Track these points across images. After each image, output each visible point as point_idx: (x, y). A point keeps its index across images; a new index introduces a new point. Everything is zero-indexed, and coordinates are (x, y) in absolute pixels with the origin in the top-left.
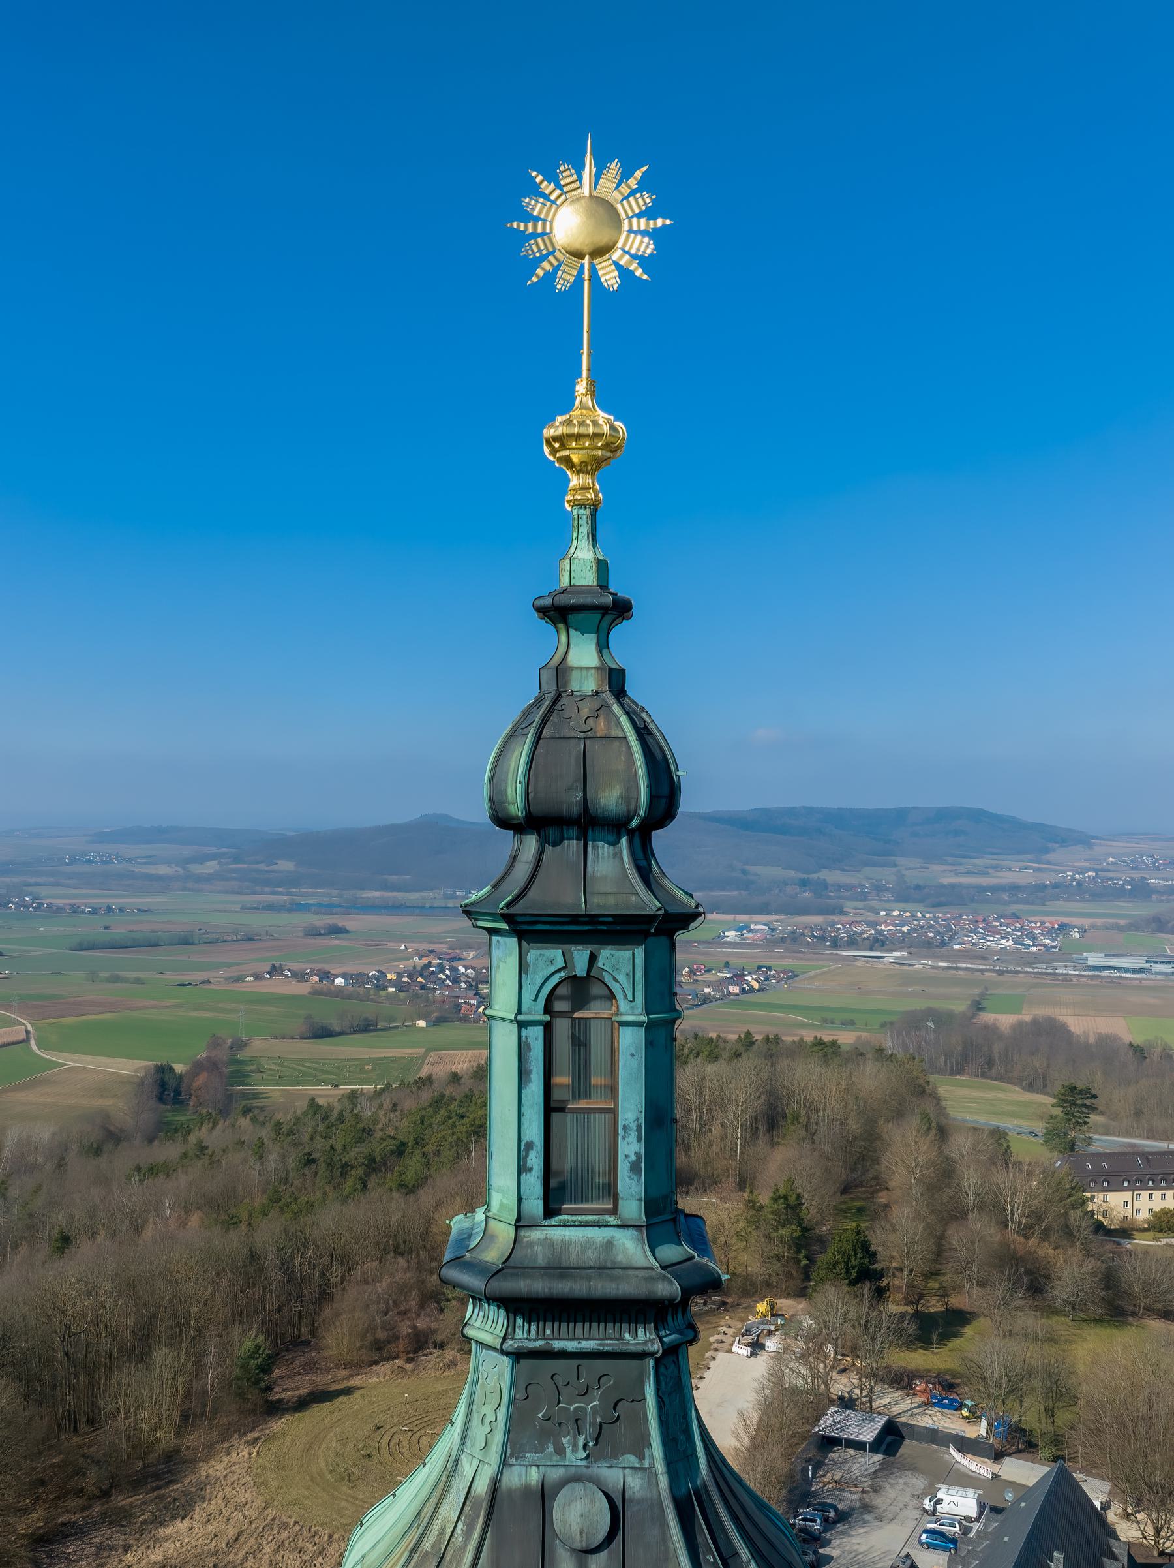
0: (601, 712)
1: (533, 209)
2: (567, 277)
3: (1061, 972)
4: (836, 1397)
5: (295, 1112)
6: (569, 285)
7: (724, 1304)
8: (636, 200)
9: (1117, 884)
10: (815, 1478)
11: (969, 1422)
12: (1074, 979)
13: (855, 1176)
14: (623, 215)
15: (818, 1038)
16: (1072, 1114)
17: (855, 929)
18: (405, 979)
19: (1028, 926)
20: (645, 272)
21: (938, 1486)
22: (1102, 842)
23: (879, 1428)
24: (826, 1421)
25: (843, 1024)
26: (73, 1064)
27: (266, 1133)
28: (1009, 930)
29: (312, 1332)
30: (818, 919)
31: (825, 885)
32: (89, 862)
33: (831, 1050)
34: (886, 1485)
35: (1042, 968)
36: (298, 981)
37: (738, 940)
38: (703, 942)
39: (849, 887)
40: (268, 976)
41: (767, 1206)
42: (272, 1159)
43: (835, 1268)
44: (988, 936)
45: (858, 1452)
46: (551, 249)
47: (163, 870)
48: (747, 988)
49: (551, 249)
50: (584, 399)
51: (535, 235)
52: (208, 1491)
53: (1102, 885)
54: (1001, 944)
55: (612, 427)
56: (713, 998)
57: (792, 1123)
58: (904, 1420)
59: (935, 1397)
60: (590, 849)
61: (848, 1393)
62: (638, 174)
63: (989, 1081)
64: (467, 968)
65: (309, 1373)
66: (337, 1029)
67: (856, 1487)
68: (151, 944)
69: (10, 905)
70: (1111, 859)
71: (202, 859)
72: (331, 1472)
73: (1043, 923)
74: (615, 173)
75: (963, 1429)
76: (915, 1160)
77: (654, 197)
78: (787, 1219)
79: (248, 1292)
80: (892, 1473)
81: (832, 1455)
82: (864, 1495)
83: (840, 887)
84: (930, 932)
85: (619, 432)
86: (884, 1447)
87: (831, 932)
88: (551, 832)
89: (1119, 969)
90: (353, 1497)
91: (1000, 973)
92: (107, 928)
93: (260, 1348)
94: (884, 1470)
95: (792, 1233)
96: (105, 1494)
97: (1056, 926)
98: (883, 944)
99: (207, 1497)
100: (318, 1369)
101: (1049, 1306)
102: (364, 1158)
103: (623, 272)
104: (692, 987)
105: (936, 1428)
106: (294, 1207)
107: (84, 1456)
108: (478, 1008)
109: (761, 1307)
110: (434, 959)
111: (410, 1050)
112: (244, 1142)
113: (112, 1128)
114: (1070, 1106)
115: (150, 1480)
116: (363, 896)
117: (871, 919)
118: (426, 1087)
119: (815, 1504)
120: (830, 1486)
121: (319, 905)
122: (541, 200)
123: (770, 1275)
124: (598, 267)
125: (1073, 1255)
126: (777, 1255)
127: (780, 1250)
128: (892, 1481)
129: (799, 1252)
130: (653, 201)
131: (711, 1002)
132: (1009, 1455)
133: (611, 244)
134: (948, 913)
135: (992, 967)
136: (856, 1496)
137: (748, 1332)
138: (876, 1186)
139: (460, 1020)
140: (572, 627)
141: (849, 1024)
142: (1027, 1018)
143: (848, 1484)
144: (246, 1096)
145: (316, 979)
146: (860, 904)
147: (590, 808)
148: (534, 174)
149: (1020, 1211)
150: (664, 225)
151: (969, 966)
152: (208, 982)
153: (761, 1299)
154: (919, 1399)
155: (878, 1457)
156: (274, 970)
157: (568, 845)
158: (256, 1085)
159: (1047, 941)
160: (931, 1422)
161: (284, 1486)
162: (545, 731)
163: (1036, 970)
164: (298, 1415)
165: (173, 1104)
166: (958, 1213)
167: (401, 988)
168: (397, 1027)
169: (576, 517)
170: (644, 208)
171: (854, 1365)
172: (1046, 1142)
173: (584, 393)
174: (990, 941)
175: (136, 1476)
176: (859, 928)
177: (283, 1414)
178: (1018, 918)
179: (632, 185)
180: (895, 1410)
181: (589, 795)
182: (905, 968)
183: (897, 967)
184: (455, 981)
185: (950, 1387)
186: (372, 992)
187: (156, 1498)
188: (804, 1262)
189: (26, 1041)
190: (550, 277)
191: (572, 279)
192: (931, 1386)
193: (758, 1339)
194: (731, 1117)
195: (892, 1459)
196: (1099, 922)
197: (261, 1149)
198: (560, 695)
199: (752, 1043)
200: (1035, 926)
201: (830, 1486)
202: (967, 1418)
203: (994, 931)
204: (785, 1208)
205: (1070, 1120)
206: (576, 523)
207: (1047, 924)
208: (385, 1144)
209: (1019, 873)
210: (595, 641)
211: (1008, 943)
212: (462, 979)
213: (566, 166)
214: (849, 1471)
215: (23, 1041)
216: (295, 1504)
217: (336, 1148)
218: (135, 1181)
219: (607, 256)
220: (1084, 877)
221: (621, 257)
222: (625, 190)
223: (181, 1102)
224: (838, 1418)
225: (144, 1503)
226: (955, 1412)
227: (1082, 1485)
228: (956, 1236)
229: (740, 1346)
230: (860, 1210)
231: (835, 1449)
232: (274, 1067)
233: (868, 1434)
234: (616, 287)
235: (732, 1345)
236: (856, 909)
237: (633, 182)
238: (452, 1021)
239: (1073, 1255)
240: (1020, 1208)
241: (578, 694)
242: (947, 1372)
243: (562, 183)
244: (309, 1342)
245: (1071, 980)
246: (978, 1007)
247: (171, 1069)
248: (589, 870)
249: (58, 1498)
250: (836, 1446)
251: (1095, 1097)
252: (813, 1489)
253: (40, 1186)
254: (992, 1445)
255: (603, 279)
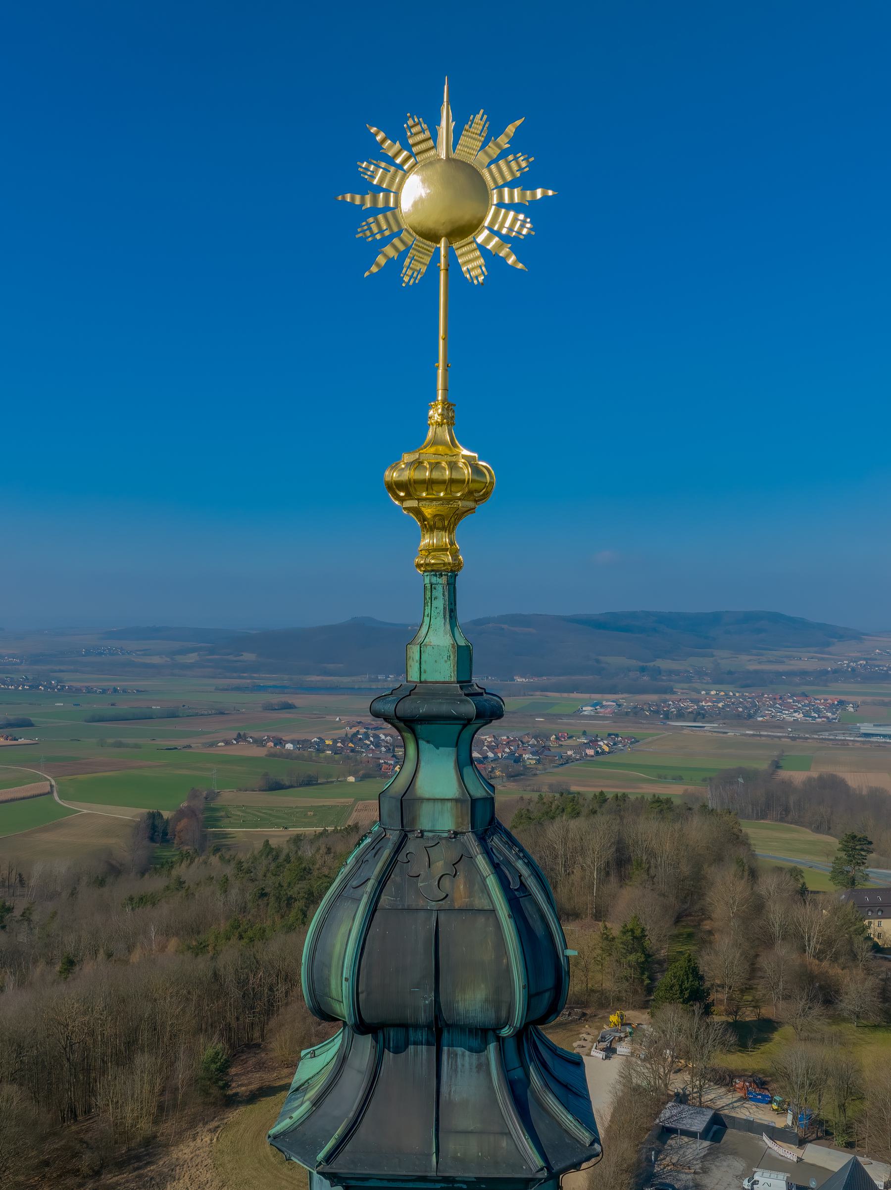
0: (460, 866)
1: (373, 177)
2: (418, 266)
3: (840, 738)
4: (672, 1093)
5: (253, 853)
6: (419, 277)
7: (584, 1014)
8: (508, 164)
9: (882, 670)
10: (658, 1161)
11: (778, 1114)
12: (850, 744)
13: (685, 906)
14: (491, 184)
15: (657, 797)
16: (853, 856)
17: (682, 705)
18: (339, 745)
19: (814, 702)
20: (519, 259)
21: (755, 1169)
22: (870, 637)
23: (708, 1120)
24: (666, 1114)
25: (674, 779)
26: (85, 811)
27: (229, 870)
28: (800, 705)
29: (262, 1036)
30: (653, 698)
31: (659, 671)
32: (100, 654)
33: (666, 806)
34: (713, 1167)
35: (825, 735)
36: (258, 746)
37: (593, 713)
38: (566, 715)
39: (677, 673)
40: (235, 742)
41: (618, 938)
42: (234, 893)
43: (672, 990)
44: (784, 710)
45: (691, 1139)
46: (395, 229)
47: (156, 660)
48: (600, 751)
49: (395, 229)
50: (439, 430)
51: (374, 211)
52: (178, 1171)
53: (871, 671)
54: (794, 717)
55: (476, 470)
56: (574, 758)
57: (637, 869)
58: (726, 1112)
59: (751, 1093)
60: (445, 1057)
61: (682, 1089)
62: (511, 129)
63: (786, 824)
64: (386, 735)
65: (259, 1071)
66: (287, 783)
67: (689, 1169)
68: (147, 717)
69: (40, 687)
70: (877, 651)
71: (184, 652)
72: (274, 1156)
73: (826, 700)
74: (481, 128)
75: (773, 1120)
76: (732, 898)
77: (532, 159)
78: (633, 947)
79: (212, 1007)
80: (718, 1157)
81: (670, 1142)
82: (696, 1176)
83: (670, 672)
84: (740, 707)
85: (485, 476)
86: (711, 1134)
87: (664, 707)
88: (392, 1034)
89: (884, 736)
90: (291, 1177)
91: (793, 739)
92: (113, 705)
93: (219, 1055)
94: (711, 1154)
95: (638, 959)
96: (97, 1174)
97: (836, 703)
98: (704, 716)
99: (177, 1178)
100: (266, 1068)
101: (839, 1015)
102: (305, 893)
103: (491, 258)
104: (558, 750)
105: (752, 1119)
106: (250, 933)
107: (82, 1141)
108: (395, 767)
109: (614, 1018)
110: (361, 729)
111: (342, 800)
112: (213, 878)
113: (114, 862)
114: (852, 850)
115: (133, 1161)
116: (307, 680)
117: (695, 697)
118: (353, 833)
119: (657, 1185)
120: (669, 1168)
121: (275, 687)
122: (383, 165)
123: (620, 992)
124: (458, 252)
125: (857, 974)
126: (626, 976)
127: (629, 972)
128: (718, 1164)
129: (642, 973)
130: (530, 165)
131: (573, 762)
132: (810, 1142)
133: (475, 222)
134: (753, 692)
135: (787, 735)
136: (689, 1176)
137: (603, 1039)
138: (702, 915)
139: (381, 776)
140: (423, 739)
141: (679, 779)
142: (815, 775)
143: (683, 1166)
144: (217, 836)
145: (271, 744)
146: (686, 686)
147: (445, 1015)
148: (373, 130)
149: (815, 939)
150: (545, 197)
151: (770, 733)
152: (189, 747)
153: (613, 1011)
154: (739, 1095)
155: (707, 1143)
156: (240, 738)
157: (416, 1052)
158: (225, 827)
159: (829, 714)
160: (748, 1113)
161: (237, 1168)
162: (383, 897)
163: (821, 737)
164: (250, 1107)
165: (162, 842)
166: (766, 941)
167: (336, 752)
168: (332, 782)
169: (428, 586)
170: (518, 174)
171: (687, 1066)
172: (833, 878)
173: (439, 420)
174: (786, 714)
175: (122, 1157)
176: (685, 704)
177: (238, 1106)
178: (806, 696)
179: (502, 144)
180: (720, 1103)
181: (442, 999)
182: (721, 735)
183: (715, 734)
184: (378, 745)
185: (762, 1084)
186: (314, 754)
187: (136, 1177)
188: (647, 981)
189: (50, 793)
190: (395, 266)
191: (424, 269)
192: (748, 1084)
193: (611, 1045)
194: (589, 863)
195: (717, 1145)
196: (869, 699)
197: (226, 884)
198: (406, 836)
199: (605, 800)
200: (820, 704)
201: (669, 1168)
202: (776, 1110)
203: (789, 707)
204: (633, 940)
205: (852, 861)
206: (428, 594)
207: (829, 701)
208: (321, 882)
209: (807, 661)
210: (453, 758)
211: (799, 716)
212: (383, 744)
213: (416, 120)
214: (684, 1155)
215: (48, 793)
216: (246, 1183)
217: (283, 884)
218: (128, 909)
219: (470, 239)
220: (857, 665)
221: (488, 240)
222: (494, 151)
223: (168, 841)
224: (675, 1112)
225: (127, 1181)
226: (767, 1105)
227: (866, 1168)
228: (766, 962)
229: (597, 1051)
230: (690, 936)
231: (673, 1136)
232: (239, 813)
233: (698, 1124)
234: (481, 279)
235: (590, 1049)
236: (683, 689)
237: (503, 141)
238: (376, 777)
239: (857, 974)
240: (815, 937)
241: (430, 834)
242: (759, 1071)
243: (411, 141)
244: (260, 1045)
245: (848, 745)
246: (777, 766)
247: (160, 815)
248: (444, 1089)
249: (60, 1176)
250: (673, 1134)
251: (870, 843)
252: (655, 1171)
253: (56, 913)
254: (797, 1134)
255: (464, 269)
